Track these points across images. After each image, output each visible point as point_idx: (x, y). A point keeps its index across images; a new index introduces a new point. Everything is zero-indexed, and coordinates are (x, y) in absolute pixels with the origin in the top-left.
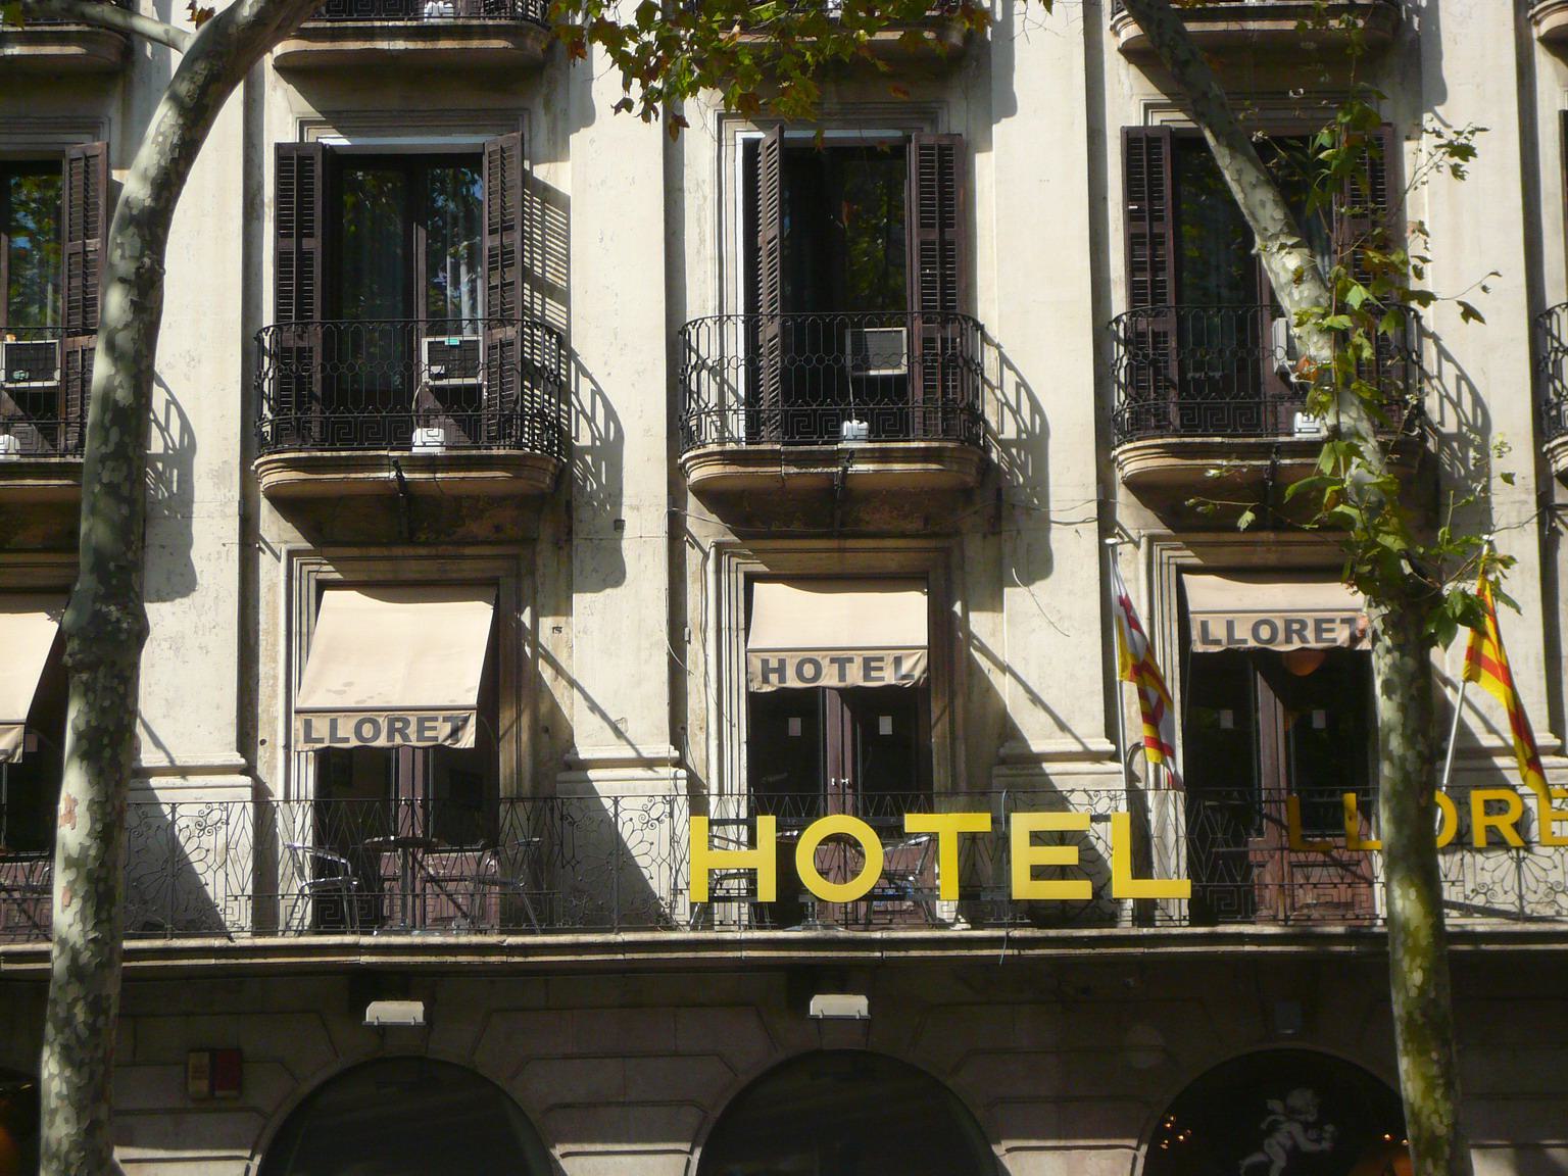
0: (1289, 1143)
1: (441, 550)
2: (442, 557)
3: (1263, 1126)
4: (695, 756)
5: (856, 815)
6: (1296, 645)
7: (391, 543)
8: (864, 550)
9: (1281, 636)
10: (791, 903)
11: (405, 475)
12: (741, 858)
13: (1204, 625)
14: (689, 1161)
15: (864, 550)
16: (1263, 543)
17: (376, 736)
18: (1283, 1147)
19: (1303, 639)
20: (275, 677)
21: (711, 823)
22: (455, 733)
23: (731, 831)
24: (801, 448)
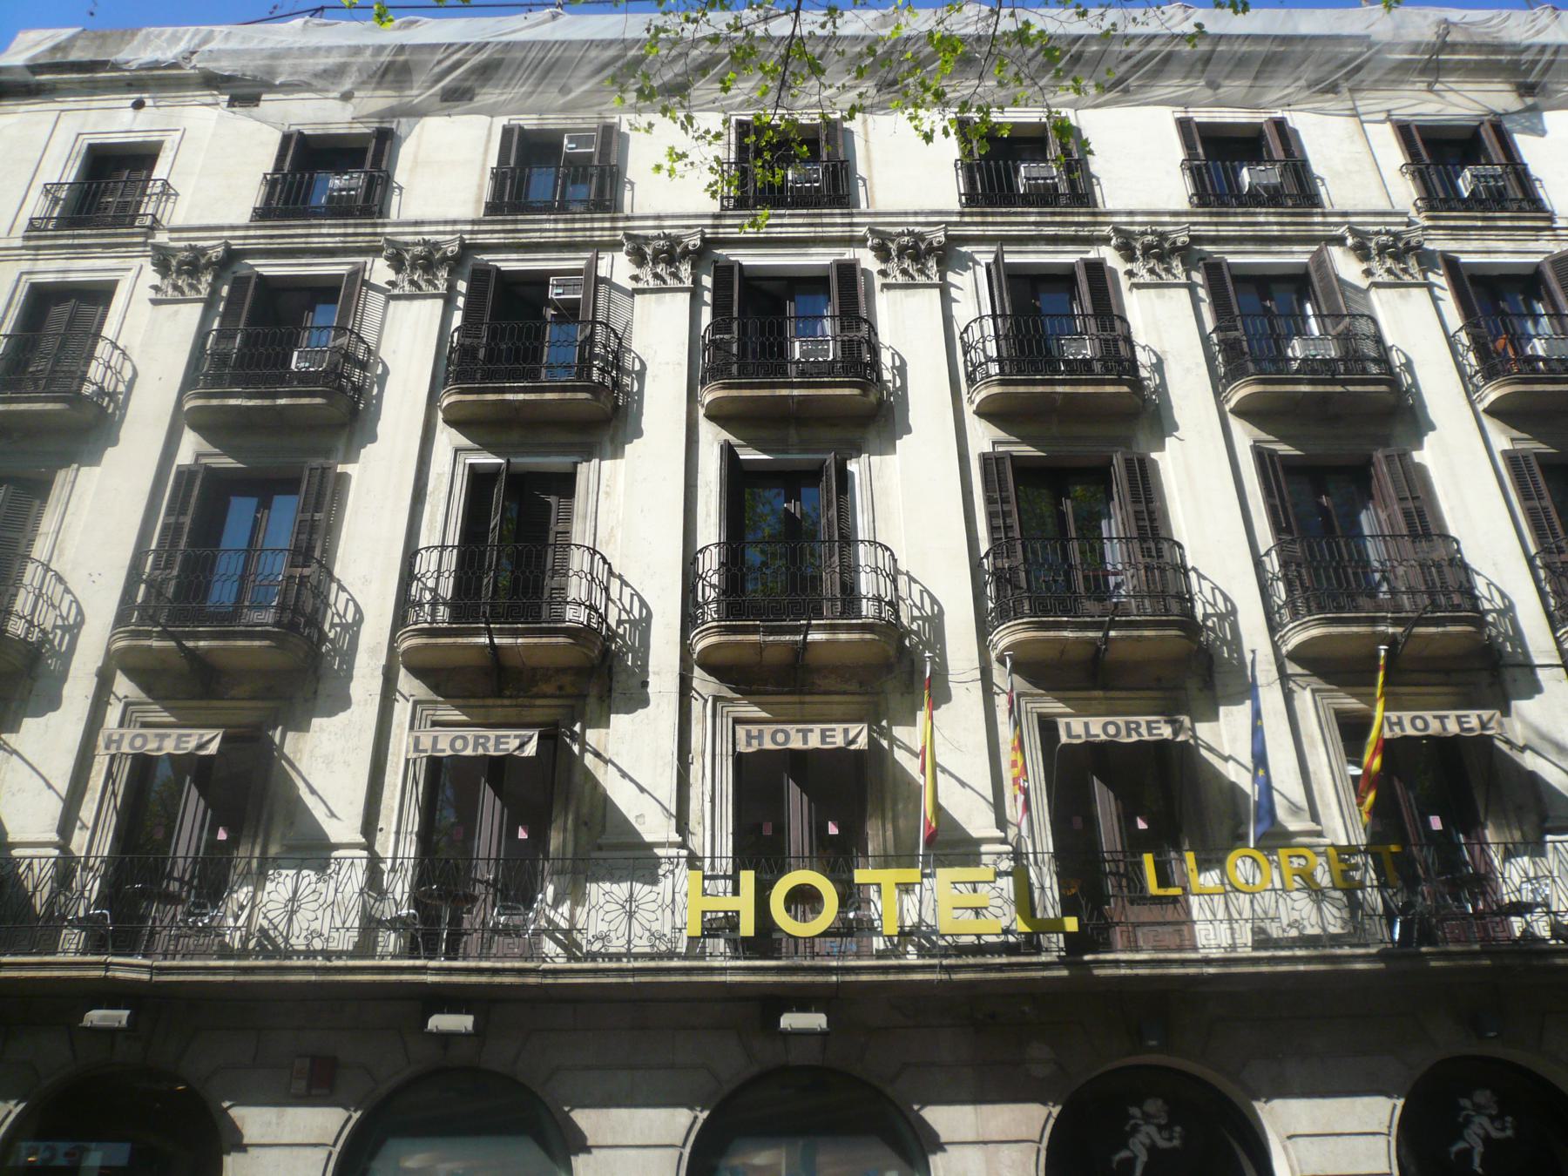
0: (1147, 1141)
1: (520, 701)
2: (520, 706)
4: (695, 843)
6: (1135, 738)
7: (484, 697)
9: (1124, 732)
10: (766, 939)
11: (496, 641)
12: (728, 903)
13: (1068, 725)
14: (681, 1154)
16: (1095, 699)
17: (465, 747)
18: (1144, 1145)
19: (1139, 734)
20: (395, 786)
21: (705, 878)
22: (522, 746)
23: (721, 883)
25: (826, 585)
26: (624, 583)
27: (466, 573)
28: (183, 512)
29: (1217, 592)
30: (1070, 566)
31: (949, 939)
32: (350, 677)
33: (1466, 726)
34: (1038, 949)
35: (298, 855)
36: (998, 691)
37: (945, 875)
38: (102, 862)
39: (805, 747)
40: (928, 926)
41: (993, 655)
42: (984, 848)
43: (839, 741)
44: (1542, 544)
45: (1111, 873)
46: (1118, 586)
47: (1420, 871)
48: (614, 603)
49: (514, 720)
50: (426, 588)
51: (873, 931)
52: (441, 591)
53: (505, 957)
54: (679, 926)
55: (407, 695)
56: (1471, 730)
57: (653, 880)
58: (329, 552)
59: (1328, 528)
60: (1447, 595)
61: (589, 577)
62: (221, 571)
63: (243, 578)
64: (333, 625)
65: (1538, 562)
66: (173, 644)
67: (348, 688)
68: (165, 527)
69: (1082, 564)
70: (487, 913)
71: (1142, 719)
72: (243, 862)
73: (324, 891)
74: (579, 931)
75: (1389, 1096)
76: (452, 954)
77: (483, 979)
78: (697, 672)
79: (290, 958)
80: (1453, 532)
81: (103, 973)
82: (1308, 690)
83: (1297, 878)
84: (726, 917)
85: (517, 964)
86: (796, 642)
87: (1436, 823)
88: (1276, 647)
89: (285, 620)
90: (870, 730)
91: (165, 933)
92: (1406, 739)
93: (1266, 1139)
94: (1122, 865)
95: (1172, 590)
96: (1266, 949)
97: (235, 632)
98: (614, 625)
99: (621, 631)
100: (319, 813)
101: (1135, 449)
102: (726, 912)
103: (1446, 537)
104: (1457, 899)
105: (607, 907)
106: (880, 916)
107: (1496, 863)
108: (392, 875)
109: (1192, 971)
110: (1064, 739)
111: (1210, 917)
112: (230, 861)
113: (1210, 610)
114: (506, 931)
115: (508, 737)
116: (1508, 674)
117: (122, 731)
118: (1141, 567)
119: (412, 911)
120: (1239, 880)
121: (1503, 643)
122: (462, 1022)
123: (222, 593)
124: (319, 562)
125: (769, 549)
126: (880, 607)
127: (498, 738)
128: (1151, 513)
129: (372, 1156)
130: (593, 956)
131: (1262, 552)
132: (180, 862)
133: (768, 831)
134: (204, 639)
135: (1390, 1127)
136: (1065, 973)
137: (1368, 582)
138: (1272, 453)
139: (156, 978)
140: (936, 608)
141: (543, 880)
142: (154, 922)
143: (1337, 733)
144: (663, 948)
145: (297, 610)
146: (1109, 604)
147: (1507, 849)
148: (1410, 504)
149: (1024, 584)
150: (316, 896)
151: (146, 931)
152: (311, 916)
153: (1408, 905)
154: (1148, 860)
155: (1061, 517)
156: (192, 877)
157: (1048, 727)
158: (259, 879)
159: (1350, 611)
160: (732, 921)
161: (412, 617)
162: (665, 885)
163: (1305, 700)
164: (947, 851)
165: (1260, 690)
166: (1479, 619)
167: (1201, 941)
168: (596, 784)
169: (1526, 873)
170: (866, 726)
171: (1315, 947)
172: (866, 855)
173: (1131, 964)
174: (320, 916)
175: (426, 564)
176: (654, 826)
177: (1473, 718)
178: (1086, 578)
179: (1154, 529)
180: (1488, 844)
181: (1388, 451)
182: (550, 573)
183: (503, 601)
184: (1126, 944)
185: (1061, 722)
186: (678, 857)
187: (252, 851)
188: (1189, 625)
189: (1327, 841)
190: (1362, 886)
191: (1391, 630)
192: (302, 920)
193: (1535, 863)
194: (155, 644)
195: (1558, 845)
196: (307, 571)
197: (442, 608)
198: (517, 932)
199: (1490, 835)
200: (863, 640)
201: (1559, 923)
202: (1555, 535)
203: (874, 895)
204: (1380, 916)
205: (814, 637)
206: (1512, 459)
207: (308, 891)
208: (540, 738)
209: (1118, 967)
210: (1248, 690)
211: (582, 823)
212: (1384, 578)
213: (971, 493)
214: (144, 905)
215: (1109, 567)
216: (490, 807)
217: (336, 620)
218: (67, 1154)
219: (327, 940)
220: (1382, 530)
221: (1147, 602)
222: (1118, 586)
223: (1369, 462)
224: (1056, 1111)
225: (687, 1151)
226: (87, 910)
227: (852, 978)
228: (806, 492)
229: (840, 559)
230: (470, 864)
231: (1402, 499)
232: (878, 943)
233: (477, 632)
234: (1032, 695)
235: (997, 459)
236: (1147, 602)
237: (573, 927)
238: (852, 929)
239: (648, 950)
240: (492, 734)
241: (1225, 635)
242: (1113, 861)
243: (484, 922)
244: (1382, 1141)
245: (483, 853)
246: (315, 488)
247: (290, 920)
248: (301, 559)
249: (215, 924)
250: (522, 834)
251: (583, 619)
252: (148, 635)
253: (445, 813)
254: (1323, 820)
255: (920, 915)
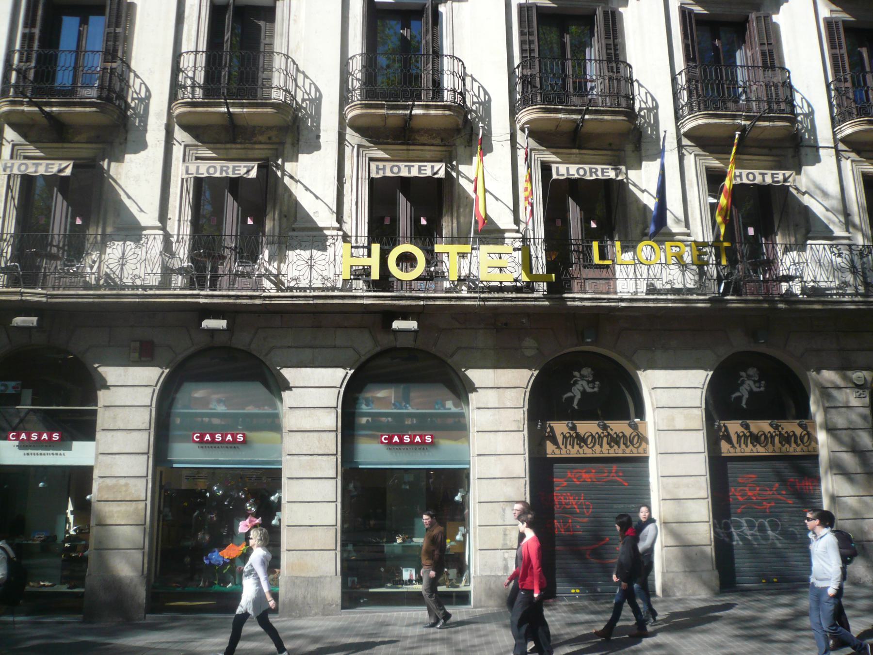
0: (581, 389)
1: (246, 146)
3: (572, 382)
4: (347, 228)
5: (411, 243)
6: (594, 177)
8: (418, 150)
9: (588, 173)
10: (385, 281)
11: (231, 110)
12: (365, 261)
13: (557, 168)
14: (339, 391)
15: (418, 150)
17: (215, 172)
19: (597, 175)
20: (176, 194)
21: (352, 247)
22: (248, 172)
23: (361, 250)
24: (393, 103)
25: (424, 81)
26: (306, 76)
27: (211, 69)
28: (33, 25)
29: (648, 95)
30: (566, 75)
31: (485, 283)
32: (146, 131)
33: (776, 179)
34: (533, 290)
35: (123, 233)
36: (520, 147)
37: (484, 249)
38: (11, 237)
39: (409, 175)
40: (474, 276)
41: (518, 126)
42: (507, 235)
43: (429, 173)
44: (836, 76)
45: (574, 251)
46: (592, 88)
47: (739, 257)
48: (300, 88)
49: (244, 157)
50: (188, 77)
51: (444, 278)
52: (197, 79)
53: (242, 289)
54: (338, 273)
55: (180, 141)
56: (778, 182)
57: (324, 248)
58: (127, 53)
59: (717, 60)
60: (778, 102)
61: (285, 73)
62: (61, 65)
63: (75, 68)
64: (133, 99)
65: (832, 87)
66: (36, 109)
67: (145, 136)
68: (24, 36)
69: (573, 75)
70: (231, 265)
71: (599, 167)
72: (93, 237)
73: (140, 253)
74: (283, 275)
75: (706, 370)
76: (213, 287)
77: (231, 301)
78: (349, 130)
79: (124, 290)
80: (787, 66)
81: (20, 298)
82: (693, 154)
83: (674, 258)
84: (364, 269)
85: (249, 293)
86: (406, 115)
87: (751, 231)
88: (678, 129)
89: (104, 95)
90: (446, 166)
91: (52, 276)
92: (743, 185)
93: (642, 389)
94: (581, 247)
95: (623, 93)
96: (653, 294)
97: (74, 102)
98: (300, 102)
99: (304, 105)
100: (134, 209)
101: (610, 5)
102: (364, 266)
103: (783, 69)
104: (756, 272)
105: (298, 263)
106: (448, 270)
107: (779, 254)
108: (177, 244)
109: (613, 304)
110: (555, 176)
111: (626, 277)
112: (84, 237)
113: (643, 106)
114: (242, 275)
115: (240, 166)
116: (804, 151)
117: (13, 161)
118: (607, 78)
119: (190, 264)
120: (643, 258)
121: (804, 133)
122: (221, 324)
123: (63, 78)
124: (121, 59)
125: (392, 57)
126: (455, 97)
127: (234, 167)
128: (615, 45)
129: (177, 391)
130: (291, 289)
131: (677, 73)
132: (56, 237)
133: (387, 221)
134: (56, 106)
135: (704, 385)
136: (547, 303)
137: (735, 92)
138: (691, 12)
139: (50, 300)
140: (487, 97)
141: (262, 248)
142: (45, 270)
143: (705, 179)
144: (329, 285)
145: (110, 89)
146: (586, 99)
147: (786, 247)
148: (766, 48)
149: (538, 85)
150: (135, 256)
151: (41, 275)
152: (134, 267)
153: (730, 274)
154: (595, 245)
155: (563, 46)
156: (64, 245)
157: (546, 168)
158: (102, 247)
159: (722, 110)
160: (367, 271)
161: (180, 95)
162: (330, 250)
163: (847, 165)
164: (487, 236)
165: (666, 153)
166: (793, 119)
167: (619, 289)
168: (290, 194)
169: (794, 261)
170: (444, 164)
171: (679, 295)
172: (441, 237)
173: (581, 299)
174: (139, 267)
175: (187, 62)
176: (324, 218)
177: (780, 175)
178: (574, 83)
179: (616, 55)
180: (777, 244)
181: (758, 14)
182: (261, 70)
183: (234, 86)
184: (580, 289)
185: (554, 167)
186: (337, 236)
187: (97, 231)
188: (631, 114)
189: (692, 239)
190: (707, 264)
191: (743, 123)
192: (129, 269)
193: (799, 255)
194: (26, 109)
195: (813, 246)
196: (114, 65)
197: (198, 89)
198: (249, 275)
199: (779, 239)
200: (444, 115)
201: (806, 287)
202: (844, 71)
203: (445, 259)
204: (715, 280)
205: (416, 112)
206: (830, 24)
207: (131, 253)
208: (258, 167)
209: (574, 301)
210: (660, 153)
211: (283, 216)
212: (745, 92)
213: (511, 28)
214: (39, 260)
215: (588, 77)
216: (231, 206)
217: (135, 96)
218: (14, 388)
219: (144, 280)
220: (747, 63)
221: (608, 99)
222: (592, 88)
223: (746, 20)
224: (536, 373)
225: (342, 390)
226: (6, 263)
227: (432, 303)
228: (414, 24)
229: (433, 65)
230: (221, 239)
231: (762, 44)
232: (446, 285)
233: (219, 105)
234: (538, 150)
235: (528, 8)
236: (608, 99)
237: (279, 274)
238: (431, 276)
239: (321, 286)
240: (231, 165)
241: (650, 121)
242: (576, 244)
243: (230, 270)
244: (699, 391)
245: (228, 233)
246: (115, 12)
247: (122, 269)
248: (110, 57)
249: (80, 271)
250: (250, 222)
251: (282, 98)
252: (21, 103)
253: (205, 207)
254: (691, 227)
255: (470, 270)
